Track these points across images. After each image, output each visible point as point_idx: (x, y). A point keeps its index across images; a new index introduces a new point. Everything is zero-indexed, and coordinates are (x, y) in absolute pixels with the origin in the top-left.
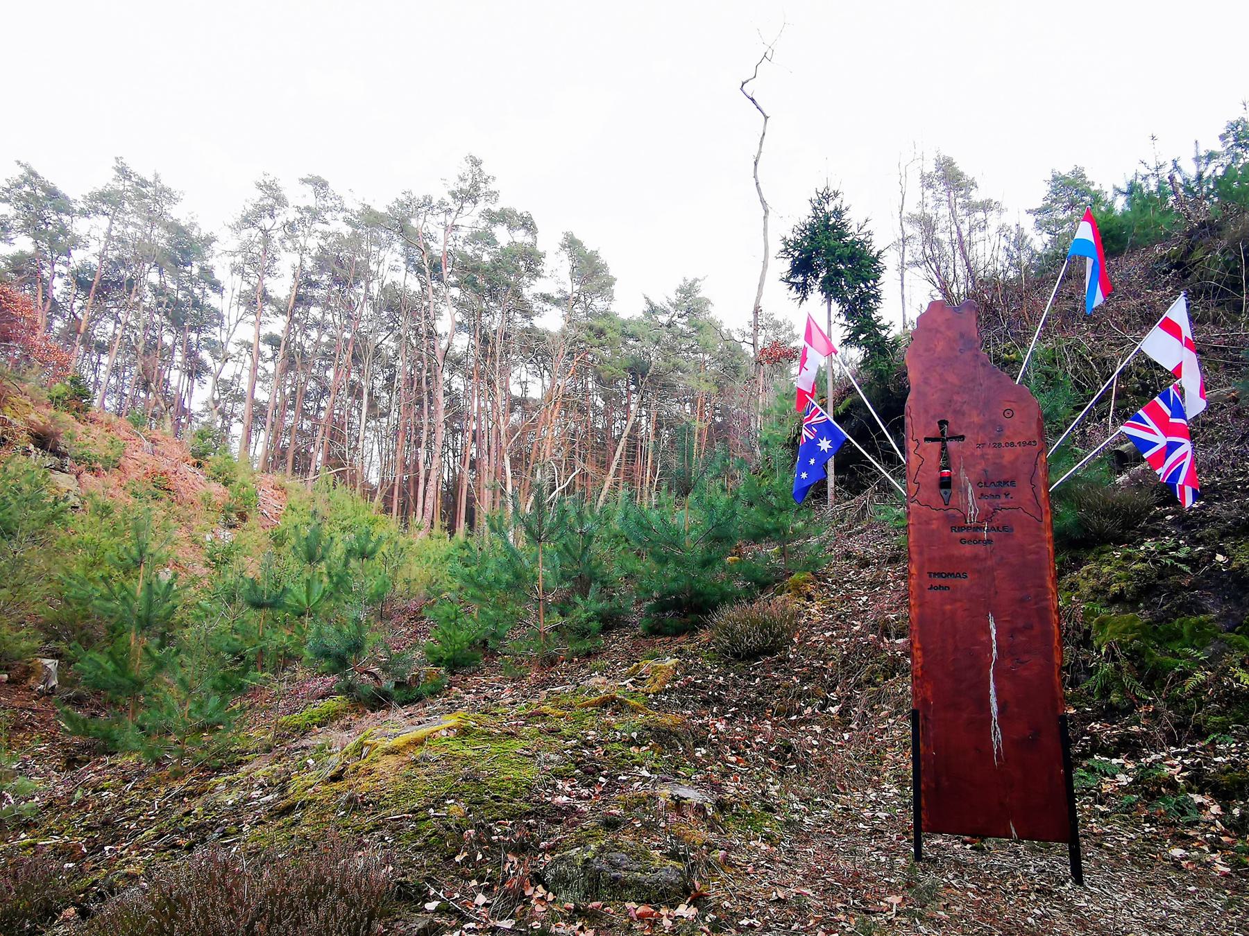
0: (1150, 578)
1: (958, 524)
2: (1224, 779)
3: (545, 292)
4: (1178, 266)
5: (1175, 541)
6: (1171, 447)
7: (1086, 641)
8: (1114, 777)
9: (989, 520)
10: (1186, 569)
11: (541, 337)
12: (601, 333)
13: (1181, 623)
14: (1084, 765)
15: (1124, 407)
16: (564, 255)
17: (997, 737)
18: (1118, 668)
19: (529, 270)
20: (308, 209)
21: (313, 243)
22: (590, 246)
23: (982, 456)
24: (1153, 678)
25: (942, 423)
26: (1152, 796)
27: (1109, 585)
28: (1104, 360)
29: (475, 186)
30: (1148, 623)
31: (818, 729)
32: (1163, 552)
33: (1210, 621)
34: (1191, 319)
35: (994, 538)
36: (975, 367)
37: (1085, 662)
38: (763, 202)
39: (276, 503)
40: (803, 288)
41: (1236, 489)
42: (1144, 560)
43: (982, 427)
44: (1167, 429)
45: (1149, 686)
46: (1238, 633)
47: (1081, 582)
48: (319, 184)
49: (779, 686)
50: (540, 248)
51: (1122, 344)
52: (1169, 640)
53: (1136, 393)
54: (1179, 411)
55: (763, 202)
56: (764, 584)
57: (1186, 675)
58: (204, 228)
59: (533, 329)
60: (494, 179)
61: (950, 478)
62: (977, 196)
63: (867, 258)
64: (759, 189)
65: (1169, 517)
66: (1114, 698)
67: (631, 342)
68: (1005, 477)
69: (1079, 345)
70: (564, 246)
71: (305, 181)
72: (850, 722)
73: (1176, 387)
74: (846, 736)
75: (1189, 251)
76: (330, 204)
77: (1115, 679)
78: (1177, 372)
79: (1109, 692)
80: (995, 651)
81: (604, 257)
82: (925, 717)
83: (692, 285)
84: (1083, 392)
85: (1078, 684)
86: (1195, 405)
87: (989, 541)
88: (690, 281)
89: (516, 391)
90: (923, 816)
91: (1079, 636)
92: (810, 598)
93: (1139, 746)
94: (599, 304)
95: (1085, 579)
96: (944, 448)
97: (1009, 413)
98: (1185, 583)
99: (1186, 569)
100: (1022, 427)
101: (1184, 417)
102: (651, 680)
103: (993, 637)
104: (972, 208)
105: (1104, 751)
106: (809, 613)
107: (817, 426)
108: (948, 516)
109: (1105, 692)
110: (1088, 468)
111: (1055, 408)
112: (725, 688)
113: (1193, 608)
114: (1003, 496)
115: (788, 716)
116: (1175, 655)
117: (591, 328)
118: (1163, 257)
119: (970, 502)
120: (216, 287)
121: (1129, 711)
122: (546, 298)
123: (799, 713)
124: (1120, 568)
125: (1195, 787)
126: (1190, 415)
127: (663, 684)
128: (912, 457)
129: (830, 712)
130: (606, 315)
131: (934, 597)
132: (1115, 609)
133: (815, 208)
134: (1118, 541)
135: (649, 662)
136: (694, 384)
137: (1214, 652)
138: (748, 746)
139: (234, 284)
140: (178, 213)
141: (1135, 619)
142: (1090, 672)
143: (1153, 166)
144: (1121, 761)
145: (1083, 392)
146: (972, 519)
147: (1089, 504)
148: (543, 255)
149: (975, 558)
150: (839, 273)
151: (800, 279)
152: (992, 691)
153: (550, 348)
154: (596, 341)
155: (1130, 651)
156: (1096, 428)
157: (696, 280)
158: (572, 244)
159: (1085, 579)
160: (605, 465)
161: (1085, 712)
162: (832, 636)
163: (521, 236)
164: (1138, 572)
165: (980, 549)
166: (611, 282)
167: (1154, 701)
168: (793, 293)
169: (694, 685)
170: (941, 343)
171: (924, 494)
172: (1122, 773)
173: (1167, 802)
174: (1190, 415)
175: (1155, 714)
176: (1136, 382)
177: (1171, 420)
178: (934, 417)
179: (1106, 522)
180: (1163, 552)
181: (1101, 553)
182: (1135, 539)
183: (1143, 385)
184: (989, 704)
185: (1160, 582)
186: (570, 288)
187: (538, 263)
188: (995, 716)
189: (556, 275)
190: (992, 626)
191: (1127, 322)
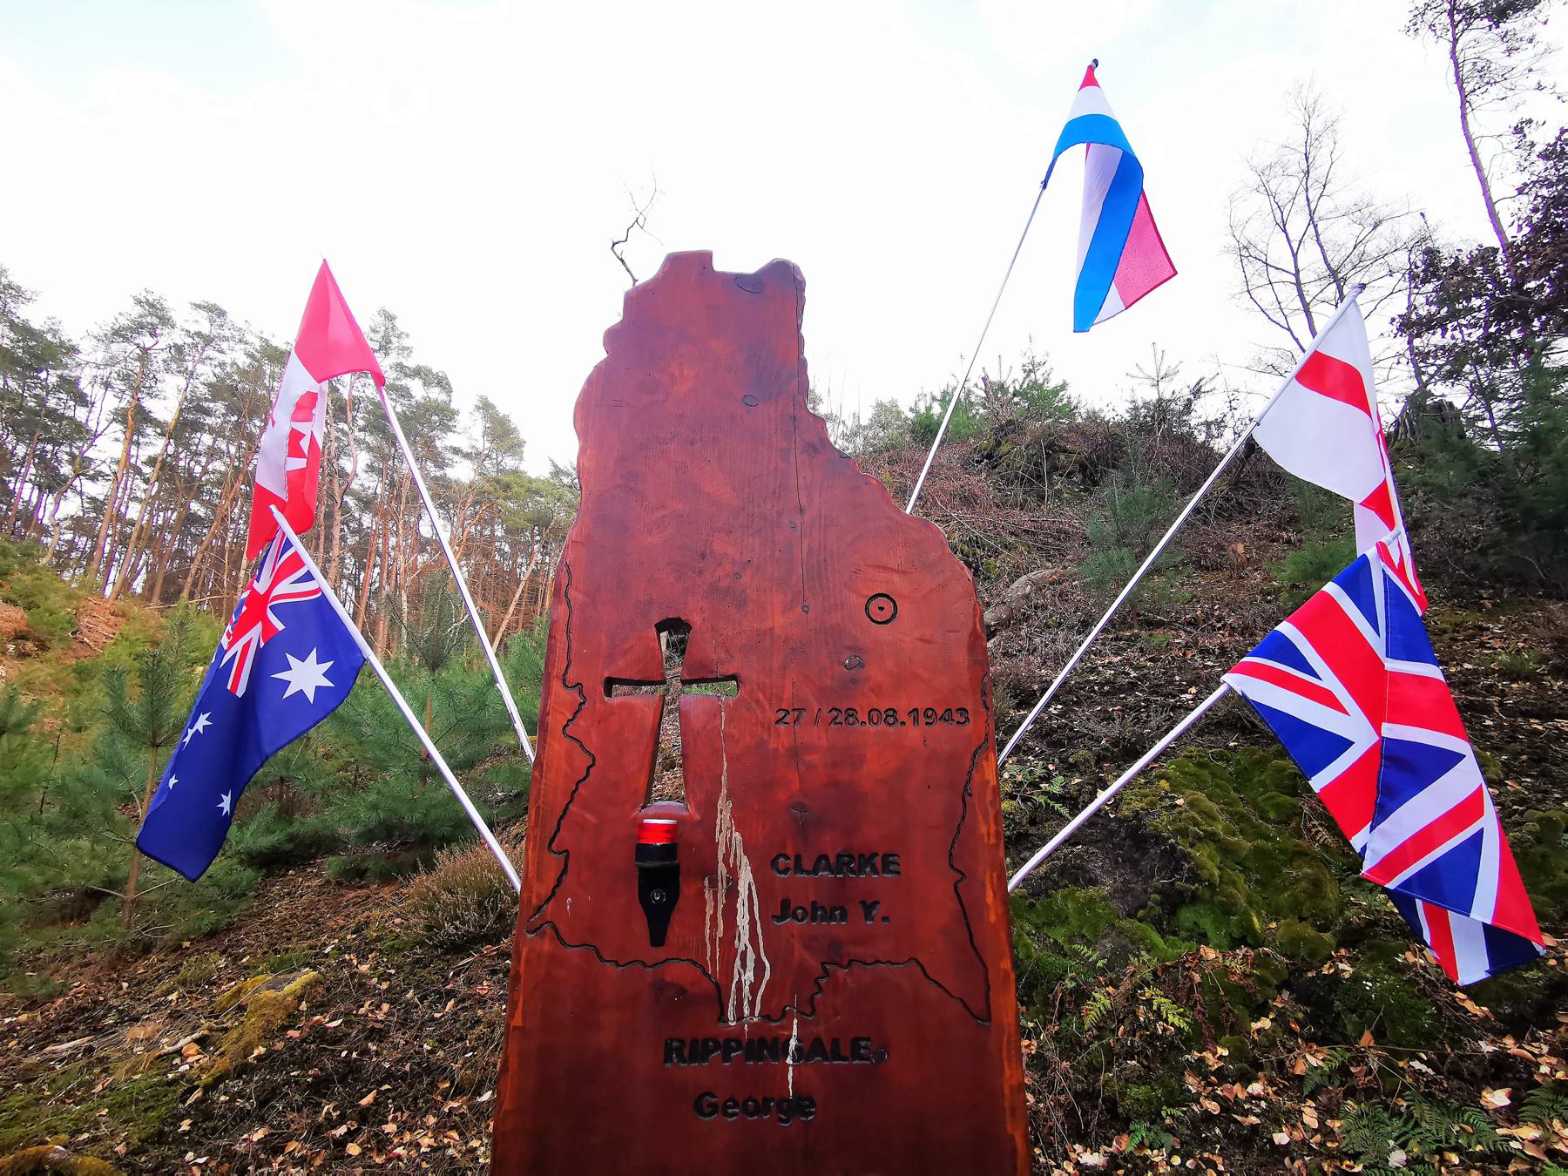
3: (456, 445)
4: (989, 456)
12: (507, 487)
16: (478, 415)
20: (199, 334)
21: (207, 373)
22: (502, 410)
23: (795, 753)
32: (1034, 785)
33: (1104, 898)
39: (108, 631)
44: (1376, 694)
46: (1141, 920)
48: (215, 312)
49: (478, 1022)
50: (453, 406)
52: (1050, 924)
57: (1081, 995)
58: (71, 332)
71: (199, 306)
75: (999, 444)
76: (228, 334)
81: (515, 421)
87: (801, 1104)
94: (509, 462)
110: (1025, 717)
112: (378, 1034)
114: (856, 912)
117: (498, 482)
120: (82, 400)
122: (456, 451)
130: (515, 472)
137: (1113, 952)
139: (109, 403)
140: (33, 315)
148: (456, 413)
154: (501, 493)
158: (486, 407)
160: (506, 605)
163: (435, 394)
166: (521, 444)
169: (321, 1034)
186: (483, 444)
189: (468, 432)
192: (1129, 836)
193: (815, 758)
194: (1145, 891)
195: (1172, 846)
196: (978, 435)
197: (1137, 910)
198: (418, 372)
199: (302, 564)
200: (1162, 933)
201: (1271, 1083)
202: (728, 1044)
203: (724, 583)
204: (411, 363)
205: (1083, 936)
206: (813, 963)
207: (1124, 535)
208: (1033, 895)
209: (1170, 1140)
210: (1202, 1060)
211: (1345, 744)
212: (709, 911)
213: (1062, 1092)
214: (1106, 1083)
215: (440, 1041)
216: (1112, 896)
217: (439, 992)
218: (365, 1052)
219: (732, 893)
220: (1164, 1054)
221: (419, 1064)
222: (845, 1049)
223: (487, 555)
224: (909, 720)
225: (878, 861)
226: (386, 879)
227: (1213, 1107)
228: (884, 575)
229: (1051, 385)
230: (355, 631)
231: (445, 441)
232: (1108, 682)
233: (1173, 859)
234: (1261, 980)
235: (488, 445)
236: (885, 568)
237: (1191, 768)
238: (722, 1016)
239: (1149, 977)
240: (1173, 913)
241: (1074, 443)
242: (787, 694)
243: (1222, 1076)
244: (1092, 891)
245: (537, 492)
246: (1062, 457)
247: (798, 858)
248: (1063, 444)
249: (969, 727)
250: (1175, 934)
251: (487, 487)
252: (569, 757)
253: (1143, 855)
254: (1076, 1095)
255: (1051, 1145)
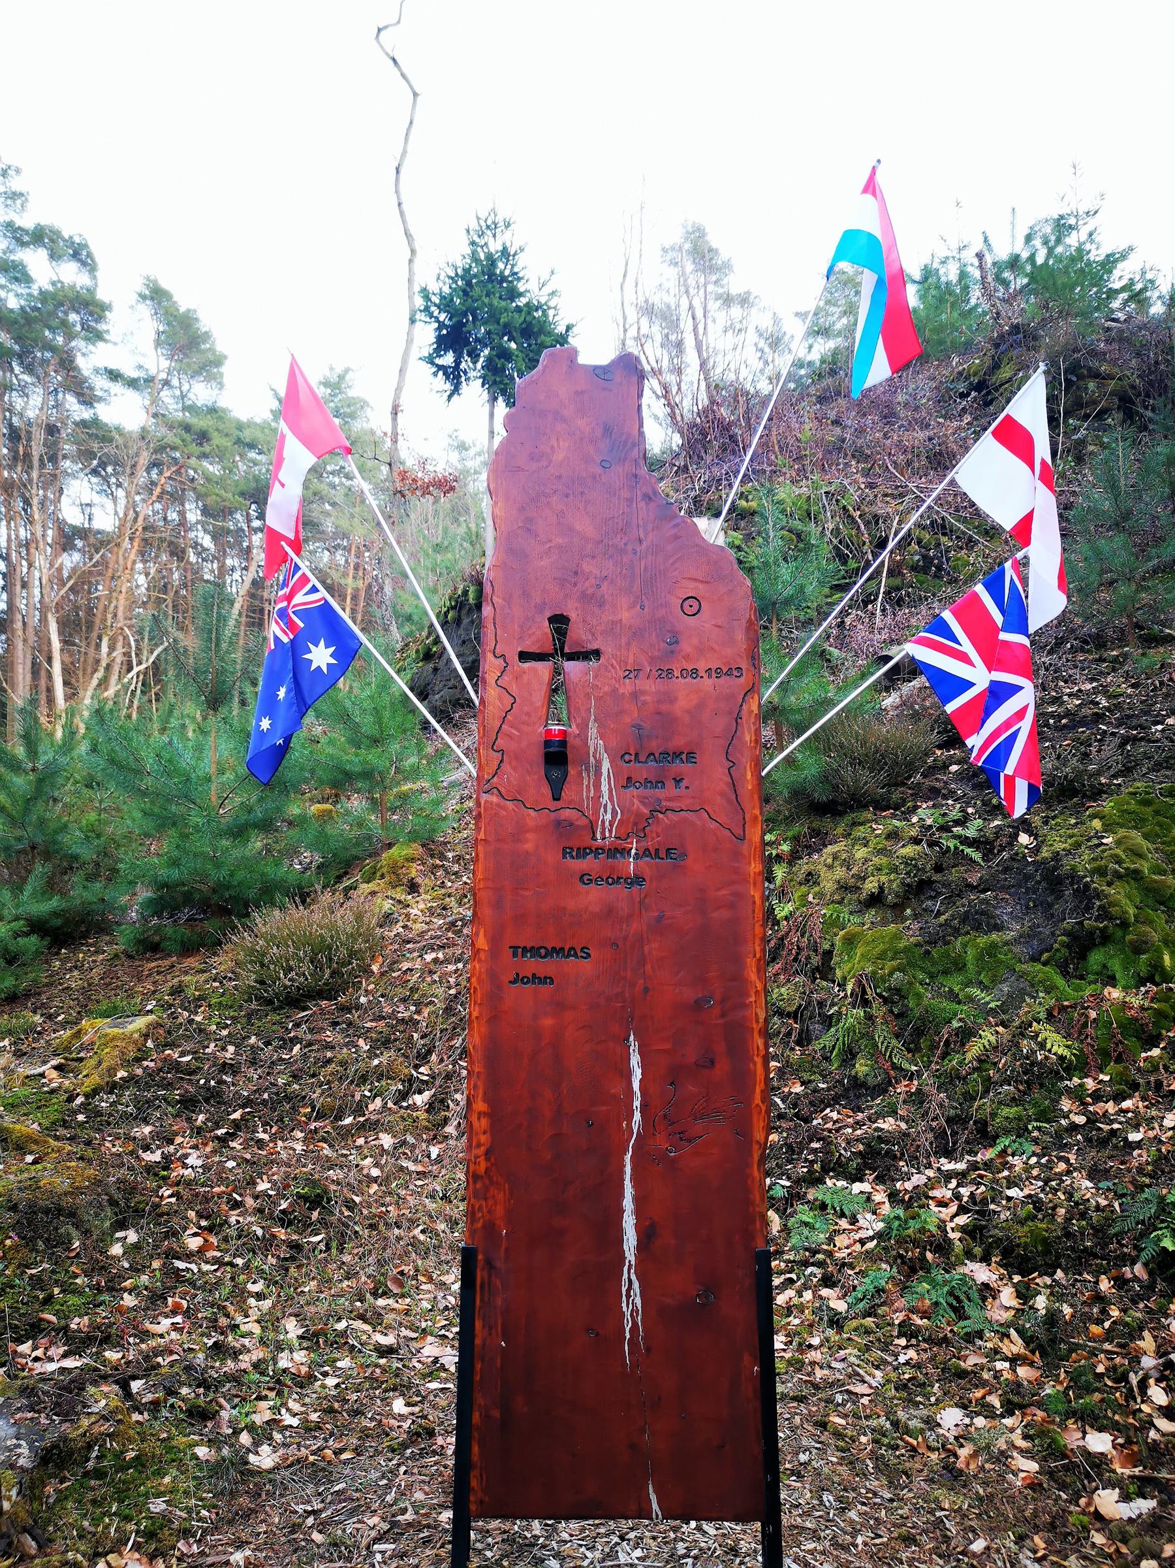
0: (923, 870)
1: (575, 839)
2: (1021, 1233)
4: (979, 387)
5: (963, 810)
6: (998, 694)
7: (824, 970)
8: (854, 1220)
9: (642, 834)
10: (976, 856)
12: (203, 437)
13: (965, 945)
14: (810, 1197)
15: (898, 589)
16: (145, 310)
17: (632, 1300)
18: (870, 1017)
19: (85, 327)
22: (184, 302)
23: (635, 695)
24: (918, 1033)
25: (559, 622)
26: (912, 1269)
27: (864, 879)
28: (876, 518)
30: (918, 945)
31: (387, 1140)
32: (945, 828)
33: (1006, 943)
34: (1053, 421)
35: (647, 873)
36: (630, 501)
37: (821, 1004)
38: (408, 234)
40: (454, 376)
41: (1047, 725)
42: (916, 841)
43: (637, 633)
44: (994, 655)
45: (912, 1048)
46: (1045, 964)
47: (823, 871)
49: (329, 1061)
50: (102, 295)
51: (902, 495)
52: (946, 972)
53: (914, 568)
54: (1018, 617)
55: (408, 234)
56: (341, 866)
57: (966, 1034)
59: (95, 422)
60: (18, 171)
61: (564, 743)
62: (735, 287)
63: (549, 334)
64: (402, 213)
65: (954, 768)
66: (861, 1067)
67: (252, 455)
68: (679, 742)
69: (843, 491)
70: (143, 297)
72: (446, 1121)
73: (1017, 565)
74: (435, 1151)
75: (996, 366)
77: (863, 1035)
78: (1023, 530)
79: (854, 1056)
80: (637, 1116)
81: (206, 322)
82: (489, 1263)
83: (341, 377)
84: (845, 563)
85: (809, 1041)
86: (1046, 603)
87: (638, 879)
89: (72, 515)
90: (474, 1483)
91: (816, 960)
92: (413, 888)
93: (895, 1158)
94: (201, 393)
95: (830, 867)
96: (557, 671)
97: (692, 605)
98: (973, 879)
99: (976, 856)
100: (714, 631)
101: (1022, 629)
102: (93, 1062)
103: (636, 1086)
104: (728, 300)
105: (839, 1169)
106: (408, 915)
107: (304, 614)
108: (558, 823)
109: (849, 1056)
111: (802, 589)
112: (231, 1068)
113: (982, 921)
114: (670, 784)
115: (339, 1118)
116: (953, 997)
117: (187, 428)
118: (960, 373)
119: (604, 794)
121: (881, 1089)
123: (359, 1109)
124: (881, 852)
125: (978, 1250)
126: (1033, 626)
127: (112, 1071)
128: (492, 693)
129: (414, 1107)
130: (213, 410)
131: (521, 998)
132: (871, 915)
133: (473, 243)
134: (881, 805)
135: (99, 1022)
136: (344, 524)
137: (1010, 995)
138: (236, 1205)
141: (897, 937)
142: (828, 1022)
143: (954, 245)
144: (866, 1187)
145: (845, 563)
146: (606, 835)
147: (842, 745)
149: (610, 912)
150: (506, 355)
151: (448, 359)
152: (628, 1203)
153: (122, 454)
154: (194, 448)
155: (889, 989)
156: (859, 618)
158: (156, 295)
159: (830, 867)
161: (815, 1091)
162: (436, 960)
164: (907, 861)
165: (620, 892)
166: (218, 361)
167: (919, 1074)
168: (442, 384)
169: (176, 1066)
170: (564, 444)
171: (510, 776)
172: (865, 1213)
173: (934, 1284)
174: (1033, 626)
175: (918, 1098)
176: (915, 553)
177: (1003, 636)
178: (540, 608)
179: (865, 776)
180: (945, 828)
181: (855, 824)
182: (904, 801)
183: (925, 557)
184: (620, 1231)
185: (937, 877)
187: (100, 319)
188: (630, 1256)
190: (635, 1060)
191: (909, 463)
192: (1044, 879)
193: (648, 698)
194: (1053, 934)
195: (1087, 885)
196: (966, 349)
197: (1041, 954)
198: (39, 237)
199: (308, 580)
200: (1065, 974)
201: (1143, 1099)
202: (597, 851)
203: (590, 592)
204: (27, 222)
205: (981, 983)
206: (646, 811)
207: (1127, 515)
208: (929, 943)
209: (1031, 1148)
210: (1081, 1085)
211: (969, 685)
212: (585, 783)
213: (936, 1118)
214: (979, 1108)
215: (294, 1076)
216: (1016, 941)
217: (282, 1039)
218: (221, 1082)
219: (598, 774)
220: (1041, 1078)
221: (277, 1094)
222: (662, 854)
223: (178, 553)
224: (705, 676)
225: (684, 756)
226: (188, 949)
227: (1080, 1120)
228: (692, 585)
229: (1096, 255)
230: (356, 629)
231: (90, 360)
232: (1068, 714)
233: (1085, 895)
234: (1159, 1013)
235: (165, 364)
236: (695, 580)
237: (1133, 806)
238: (594, 838)
239: (1043, 1016)
240: (1083, 957)
241: (1114, 362)
242: (631, 661)
243: (1097, 1097)
244: (994, 936)
245: (252, 446)
246: (1092, 385)
247: (637, 754)
248: (1093, 363)
249: (742, 679)
250: (1082, 978)
251: (171, 438)
252: (500, 698)
253: (1057, 898)
254: (949, 1121)
255: (917, 1158)
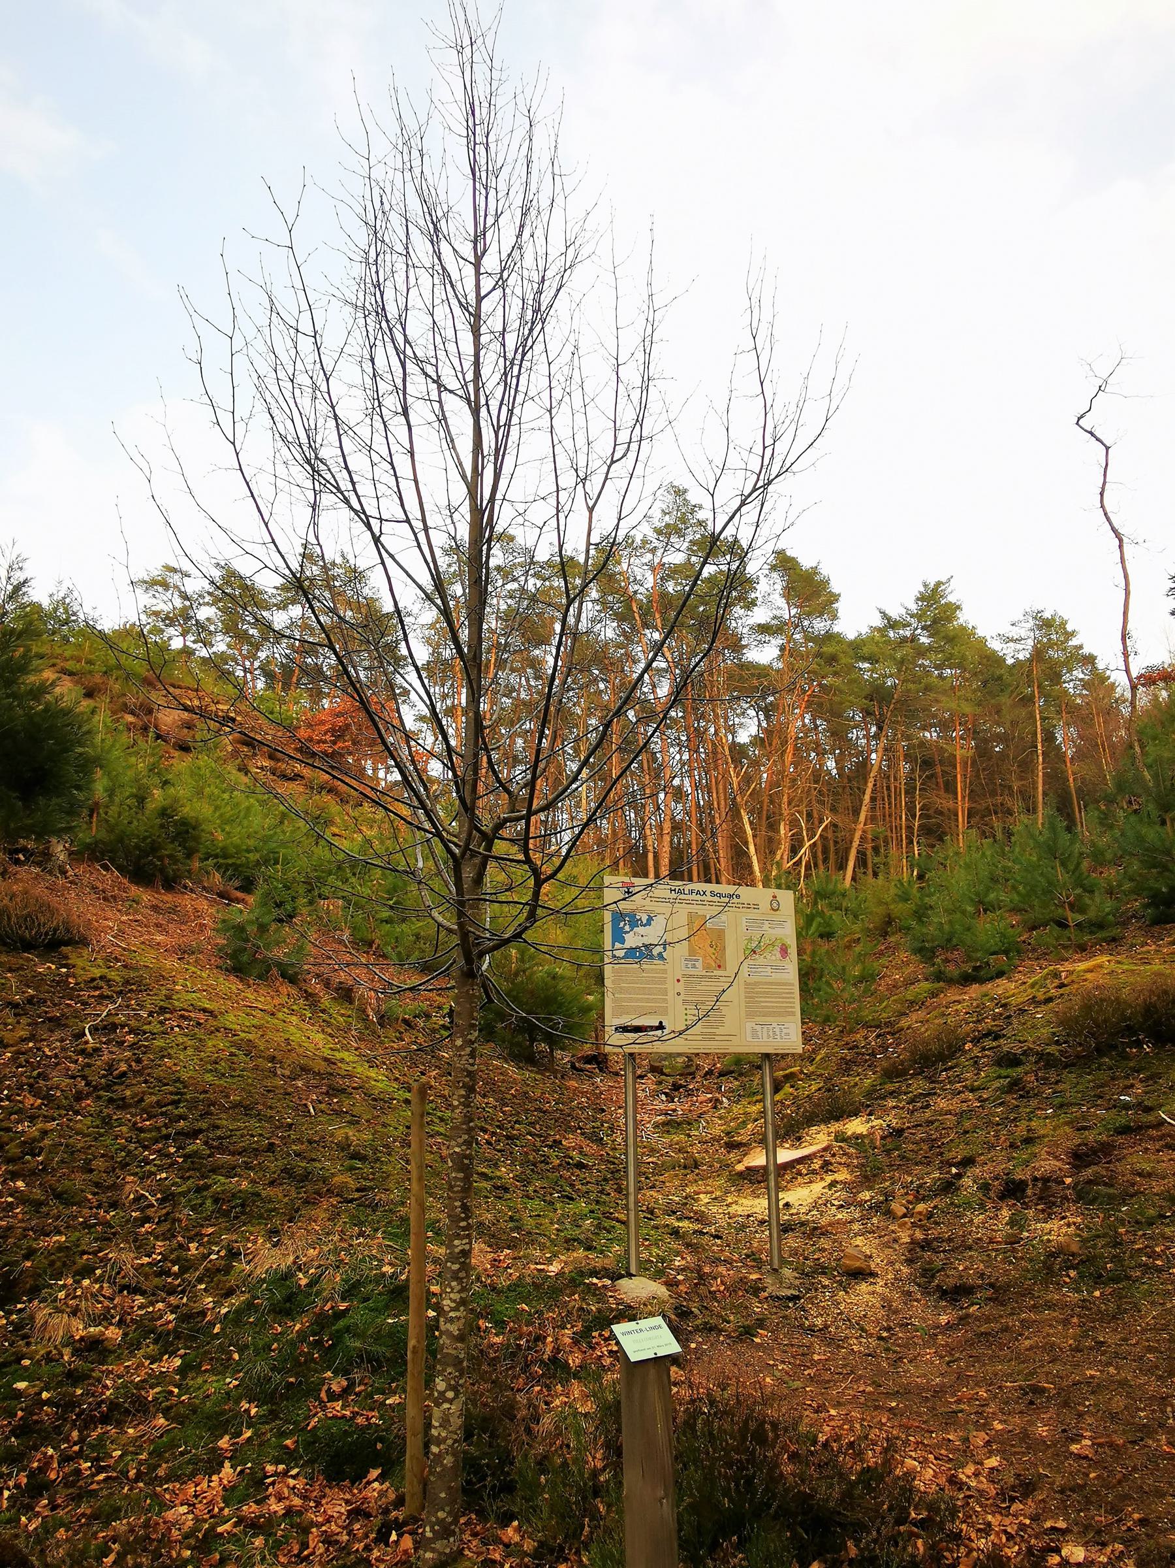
11: (762, 671)
29: (683, 519)
70: (773, 568)
88: (932, 586)
94: (820, 626)
157: (939, 584)
158: (784, 563)
189: (770, 600)
